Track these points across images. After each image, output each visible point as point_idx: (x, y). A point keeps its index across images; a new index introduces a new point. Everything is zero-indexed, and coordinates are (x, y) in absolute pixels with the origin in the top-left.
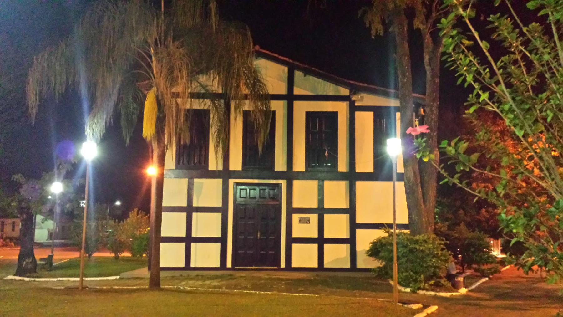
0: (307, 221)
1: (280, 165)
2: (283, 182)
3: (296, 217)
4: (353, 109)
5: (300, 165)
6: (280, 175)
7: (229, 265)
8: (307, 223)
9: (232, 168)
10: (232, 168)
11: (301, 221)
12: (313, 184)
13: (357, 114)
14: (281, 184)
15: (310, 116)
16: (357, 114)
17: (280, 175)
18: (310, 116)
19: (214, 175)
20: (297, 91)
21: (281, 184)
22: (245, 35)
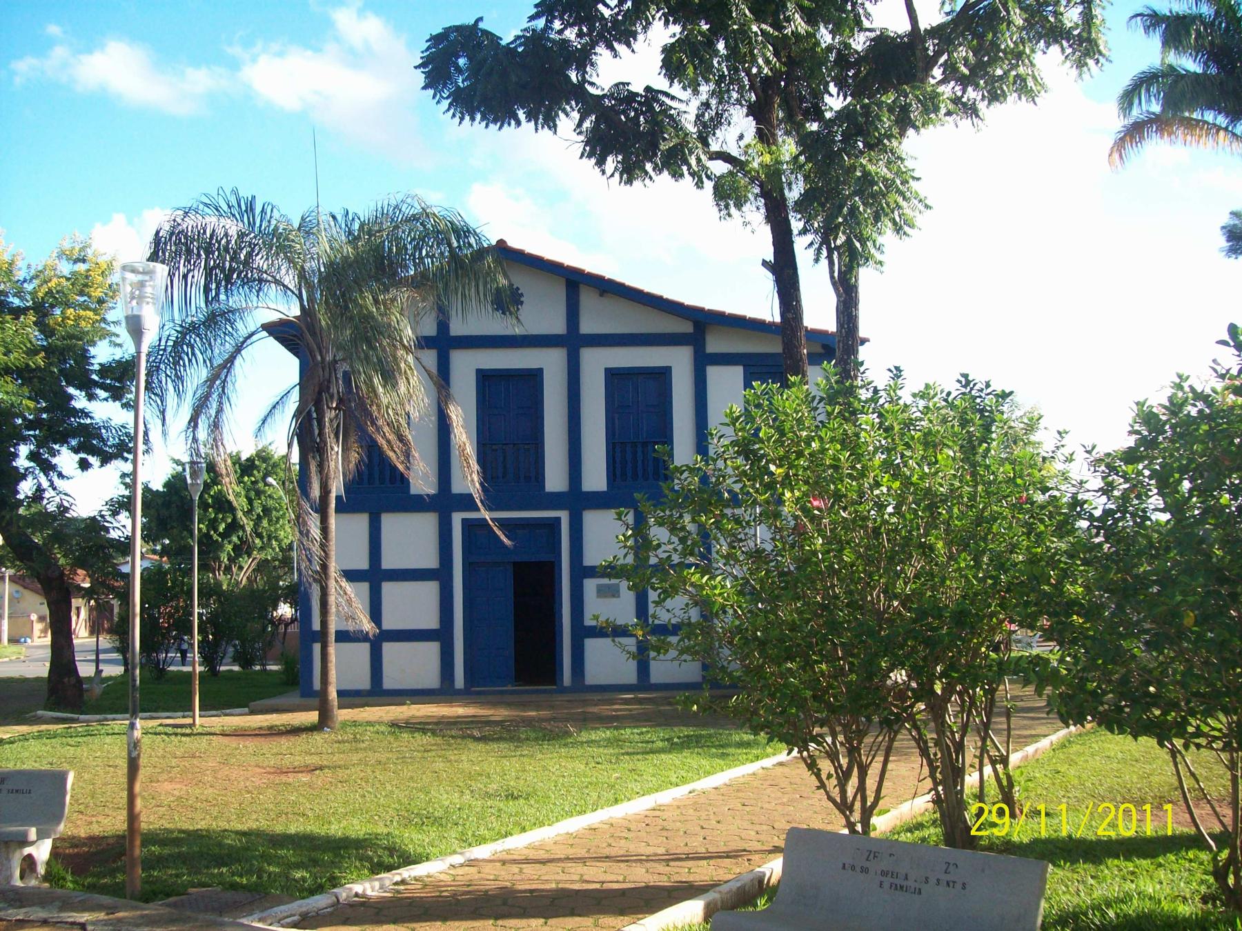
0: (613, 592)
1: (555, 479)
2: (564, 515)
3: (590, 585)
4: (702, 361)
5: (595, 478)
6: (555, 501)
7: (459, 681)
8: (613, 596)
9: (457, 488)
10: (457, 488)
11: (602, 592)
12: (360, 522)
13: (388, 684)
14: (539, 372)
15: (614, 376)
16: (388, 684)
17: (555, 501)
18: (614, 376)
19: (417, 504)
20: (588, 326)
21: (539, 372)
22: (427, 50)
